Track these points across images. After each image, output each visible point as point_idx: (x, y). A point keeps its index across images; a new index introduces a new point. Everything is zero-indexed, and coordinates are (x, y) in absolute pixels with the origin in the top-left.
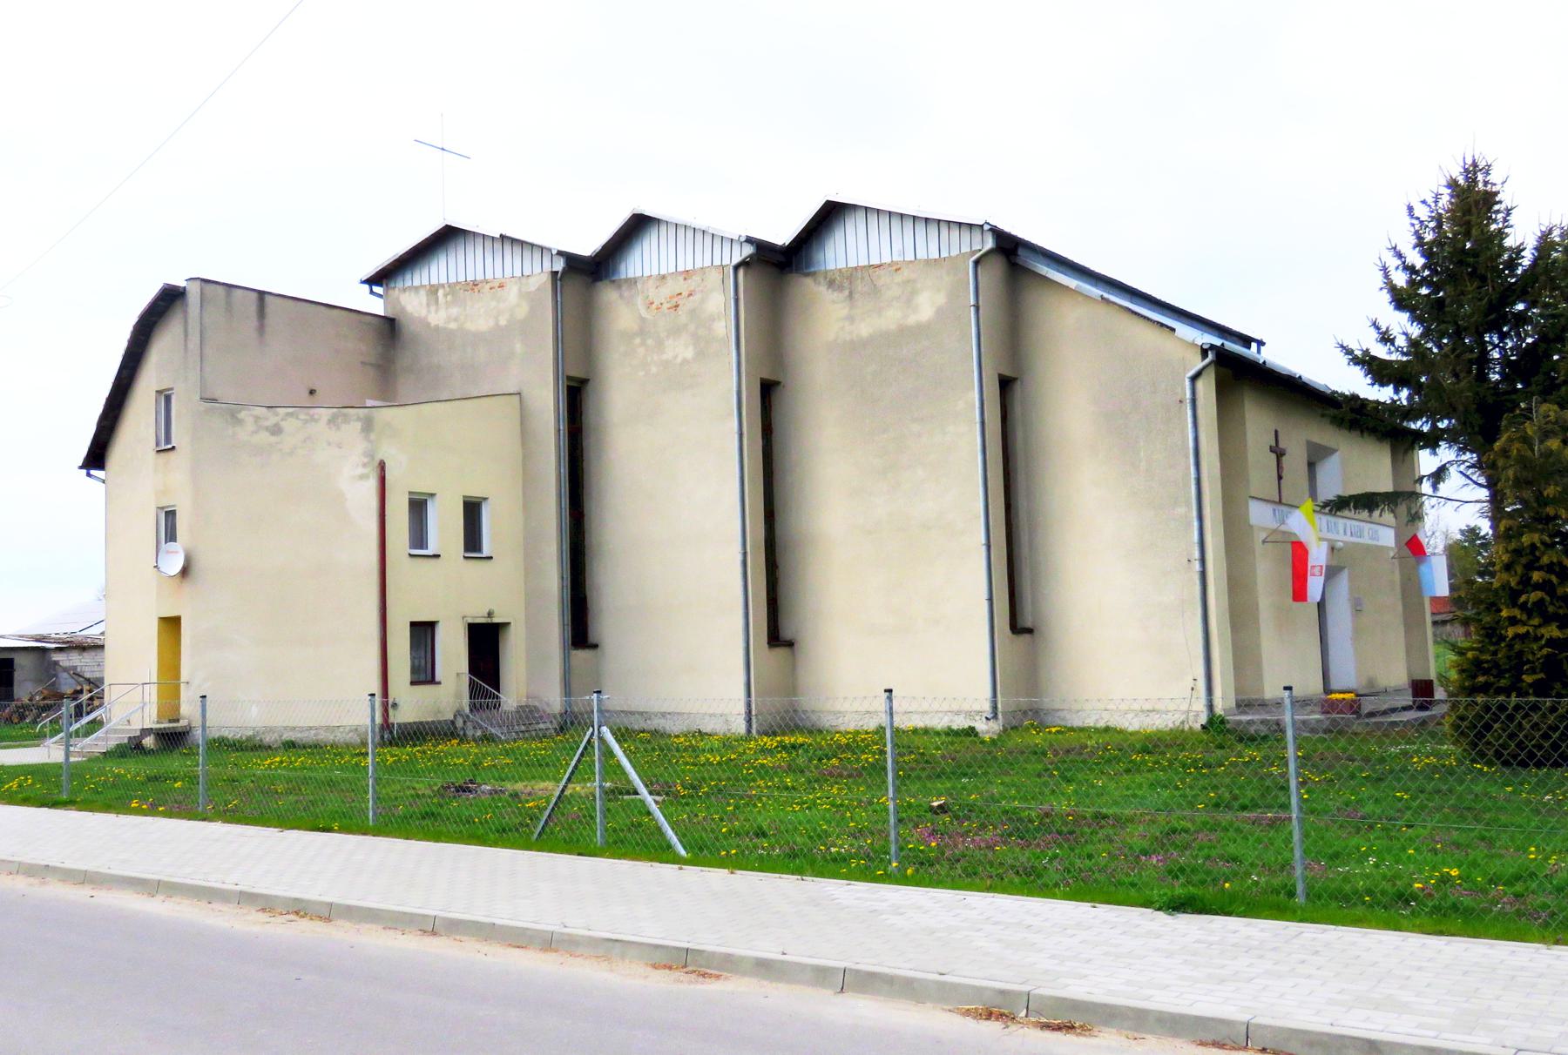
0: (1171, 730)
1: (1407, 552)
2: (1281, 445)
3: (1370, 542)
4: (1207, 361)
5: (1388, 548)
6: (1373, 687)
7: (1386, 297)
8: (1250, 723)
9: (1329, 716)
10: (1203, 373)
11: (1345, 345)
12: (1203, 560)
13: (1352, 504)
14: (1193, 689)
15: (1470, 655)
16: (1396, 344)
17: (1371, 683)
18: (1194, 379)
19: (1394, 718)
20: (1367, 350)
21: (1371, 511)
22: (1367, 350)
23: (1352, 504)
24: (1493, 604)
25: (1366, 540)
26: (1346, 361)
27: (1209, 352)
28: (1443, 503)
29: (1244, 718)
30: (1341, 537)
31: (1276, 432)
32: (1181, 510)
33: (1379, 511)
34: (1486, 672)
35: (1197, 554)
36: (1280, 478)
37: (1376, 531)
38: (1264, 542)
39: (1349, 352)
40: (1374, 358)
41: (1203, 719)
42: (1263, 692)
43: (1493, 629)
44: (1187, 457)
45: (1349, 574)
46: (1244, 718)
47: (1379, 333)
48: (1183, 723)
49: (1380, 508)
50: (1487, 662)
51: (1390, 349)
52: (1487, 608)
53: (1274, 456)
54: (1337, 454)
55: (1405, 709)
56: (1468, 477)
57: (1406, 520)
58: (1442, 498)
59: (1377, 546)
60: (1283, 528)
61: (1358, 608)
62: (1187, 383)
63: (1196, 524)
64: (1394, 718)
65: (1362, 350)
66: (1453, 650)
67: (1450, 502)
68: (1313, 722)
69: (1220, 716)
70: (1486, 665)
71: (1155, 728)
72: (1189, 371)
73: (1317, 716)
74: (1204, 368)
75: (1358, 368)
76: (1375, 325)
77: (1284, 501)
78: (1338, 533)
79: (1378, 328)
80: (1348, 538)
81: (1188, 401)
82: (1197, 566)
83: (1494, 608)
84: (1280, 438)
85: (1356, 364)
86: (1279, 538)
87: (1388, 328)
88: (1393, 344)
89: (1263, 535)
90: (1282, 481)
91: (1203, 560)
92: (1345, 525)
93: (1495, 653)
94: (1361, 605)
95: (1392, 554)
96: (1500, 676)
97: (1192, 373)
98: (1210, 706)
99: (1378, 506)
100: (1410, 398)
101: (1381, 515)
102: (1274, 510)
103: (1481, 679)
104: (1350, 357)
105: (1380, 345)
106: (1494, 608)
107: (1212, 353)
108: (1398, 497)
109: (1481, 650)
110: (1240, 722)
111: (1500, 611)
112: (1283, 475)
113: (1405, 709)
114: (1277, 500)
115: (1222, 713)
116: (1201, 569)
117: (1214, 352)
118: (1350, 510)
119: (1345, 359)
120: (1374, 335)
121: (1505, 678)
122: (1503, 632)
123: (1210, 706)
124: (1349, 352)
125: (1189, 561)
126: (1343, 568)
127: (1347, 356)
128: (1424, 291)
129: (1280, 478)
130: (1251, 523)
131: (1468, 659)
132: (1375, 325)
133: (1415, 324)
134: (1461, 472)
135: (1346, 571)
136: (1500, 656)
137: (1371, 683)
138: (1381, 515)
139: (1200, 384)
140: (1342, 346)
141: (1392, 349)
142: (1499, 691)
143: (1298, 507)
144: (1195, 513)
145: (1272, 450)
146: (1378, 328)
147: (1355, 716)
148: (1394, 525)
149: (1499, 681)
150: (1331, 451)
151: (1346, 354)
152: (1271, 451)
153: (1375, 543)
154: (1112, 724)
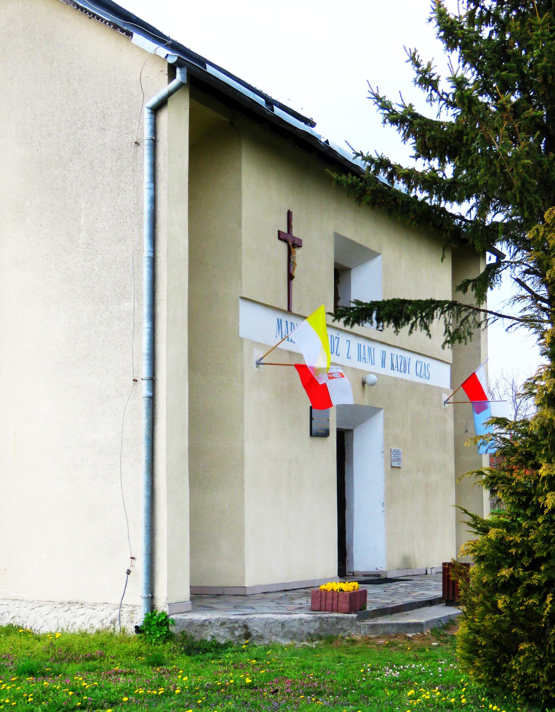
0: (98, 632)
1: (463, 395)
2: (295, 233)
3: (418, 380)
4: (175, 83)
5: (440, 390)
6: (409, 568)
7: (433, 29)
8: (203, 625)
9: (319, 615)
10: (170, 100)
11: (381, 96)
12: (153, 380)
13: (374, 315)
14: (129, 572)
15: (492, 534)
16: (440, 89)
17: (407, 562)
18: (156, 110)
19: (412, 618)
20: (411, 105)
21: (397, 325)
22: (411, 105)
23: (374, 315)
24: (530, 456)
25: (411, 377)
26: (381, 118)
27: (178, 70)
28: (492, 320)
29: (199, 617)
30: (377, 368)
31: (289, 214)
32: (128, 305)
33: (410, 326)
34: (513, 562)
35: (145, 372)
36: (290, 277)
37: (427, 367)
38: (258, 364)
39: (385, 105)
40: (416, 116)
41: (139, 619)
42: (243, 578)
43: (529, 494)
44: (141, 227)
45: (385, 419)
46: (199, 617)
47: (418, 72)
48: (113, 622)
49: (411, 322)
50: (516, 545)
51: (431, 94)
52: (520, 461)
53: (283, 247)
54: (379, 259)
55: (431, 603)
56: (523, 285)
57: (443, 339)
58: (491, 312)
59: (426, 385)
60: (286, 345)
61: (395, 464)
62: (147, 115)
63: (146, 325)
64: (412, 618)
65: (404, 106)
66: (474, 526)
67: (501, 319)
68: (296, 624)
69: (163, 613)
70: (513, 551)
71: (76, 627)
72: (150, 98)
73: (304, 616)
74: (170, 94)
75: (395, 127)
76: (415, 61)
77: (294, 310)
78: (373, 363)
79: (418, 65)
80: (387, 371)
81: (146, 142)
82: (144, 389)
83: (530, 463)
84: (294, 223)
85: (394, 122)
86: (285, 360)
87: (429, 65)
88: (435, 89)
89: (258, 354)
90: (294, 282)
91: (153, 380)
92: (384, 353)
93: (527, 533)
94: (399, 460)
95: (445, 397)
96: (535, 566)
97: (153, 100)
98: (151, 599)
99: (408, 319)
100: (456, 173)
101: (410, 332)
102: (279, 322)
103: (505, 572)
104: (386, 112)
105: (418, 89)
106: (530, 463)
107: (181, 73)
108: (435, 308)
109: (509, 528)
110: (191, 623)
111: (537, 466)
112: (296, 273)
113: (431, 603)
114: (286, 308)
115: (166, 610)
116: (150, 394)
117: (185, 70)
118: (372, 323)
119: (379, 115)
120: (412, 73)
121: (540, 571)
122: (541, 500)
123: (151, 599)
124: (385, 105)
125: (135, 380)
126: (377, 410)
127: (381, 111)
128: (486, 32)
129: (290, 277)
130: (241, 336)
131: (489, 540)
132: (415, 61)
133: (467, 66)
134: (517, 280)
135: (382, 412)
136: (532, 537)
137: (407, 562)
138: (410, 332)
139: (164, 116)
140: (377, 97)
141: (435, 95)
142: (530, 590)
143: (305, 318)
144: (145, 310)
145: (281, 237)
146: (418, 65)
147: (354, 615)
148: (451, 362)
149: (532, 575)
150: (370, 255)
151: (382, 108)
152: (280, 238)
153: (423, 381)
154: (17, 622)
